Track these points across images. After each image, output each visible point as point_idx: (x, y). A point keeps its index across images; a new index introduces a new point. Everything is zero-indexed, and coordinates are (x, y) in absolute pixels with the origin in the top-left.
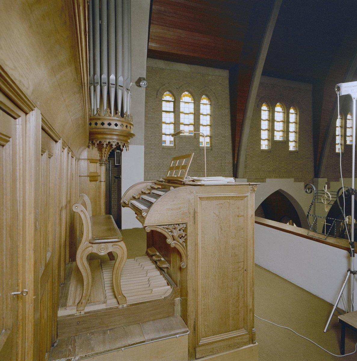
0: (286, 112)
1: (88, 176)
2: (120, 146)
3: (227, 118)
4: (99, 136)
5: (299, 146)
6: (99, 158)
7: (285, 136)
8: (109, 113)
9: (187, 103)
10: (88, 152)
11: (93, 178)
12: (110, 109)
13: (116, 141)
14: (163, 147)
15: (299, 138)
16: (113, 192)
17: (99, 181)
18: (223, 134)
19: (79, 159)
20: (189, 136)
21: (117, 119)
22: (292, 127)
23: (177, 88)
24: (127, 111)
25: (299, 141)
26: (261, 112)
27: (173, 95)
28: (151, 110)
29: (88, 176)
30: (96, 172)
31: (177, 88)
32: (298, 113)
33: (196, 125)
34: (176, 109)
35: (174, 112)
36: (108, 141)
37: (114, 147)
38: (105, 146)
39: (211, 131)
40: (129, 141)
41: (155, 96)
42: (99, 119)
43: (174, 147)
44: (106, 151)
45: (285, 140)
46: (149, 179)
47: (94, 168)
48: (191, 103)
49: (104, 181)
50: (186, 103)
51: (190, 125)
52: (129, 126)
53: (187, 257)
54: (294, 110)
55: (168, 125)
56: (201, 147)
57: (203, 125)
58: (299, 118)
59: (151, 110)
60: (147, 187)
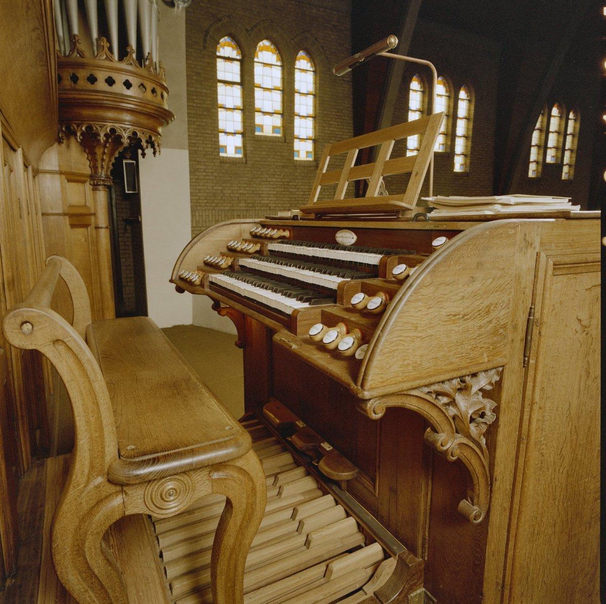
0: (453, 95)
1: (65, 214)
2: (140, 140)
3: (347, 102)
4: (86, 112)
5: (471, 163)
6: (88, 171)
7: (449, 143)
8: (106, 49)
9: (267, 64)
10: (60, 154)
11: (79, 219)
12: (109, 40)
13: (130, 127)
14: (221, 159)
15: (472, 148)
16: (123, 252)
17: (93, 226)
18: (338, 136)
19: (36, 172)
20: (272, 137)
21: (130, 68)
22: (461, 127)
23: (247, 30)
24: (151, 49)
25: (472, 153)
26: (408, 94)
27: (239, 46)
28: (195, 78)
29: (65, 214)
30: (85, 206)
31: (247, 30)
32: (473, 100)
33: (286, 114)
34: (246, 78)
35: (241, 84)
36: (109, 125)
37: (126, 141)
38: (102, 138)
39: (315, 128)
40: (160, 130)
41: (202, 44)
42: (82, 66)
43: (244, 160)
44: (104, 153)
45: (449, 151)
46: (196, 224)
47: (79, 194)
48: (276, 65)
49: (107, 228)
50: (265, 64)
51: (274, 115)
52: (159, 90)
53: (491, 485)
54: (466, 92)
55: (229, 113)
56: (297, 161)
57: (300, 116)
58: (475, 110)
59: (195, 78)
60: (241, 234)
